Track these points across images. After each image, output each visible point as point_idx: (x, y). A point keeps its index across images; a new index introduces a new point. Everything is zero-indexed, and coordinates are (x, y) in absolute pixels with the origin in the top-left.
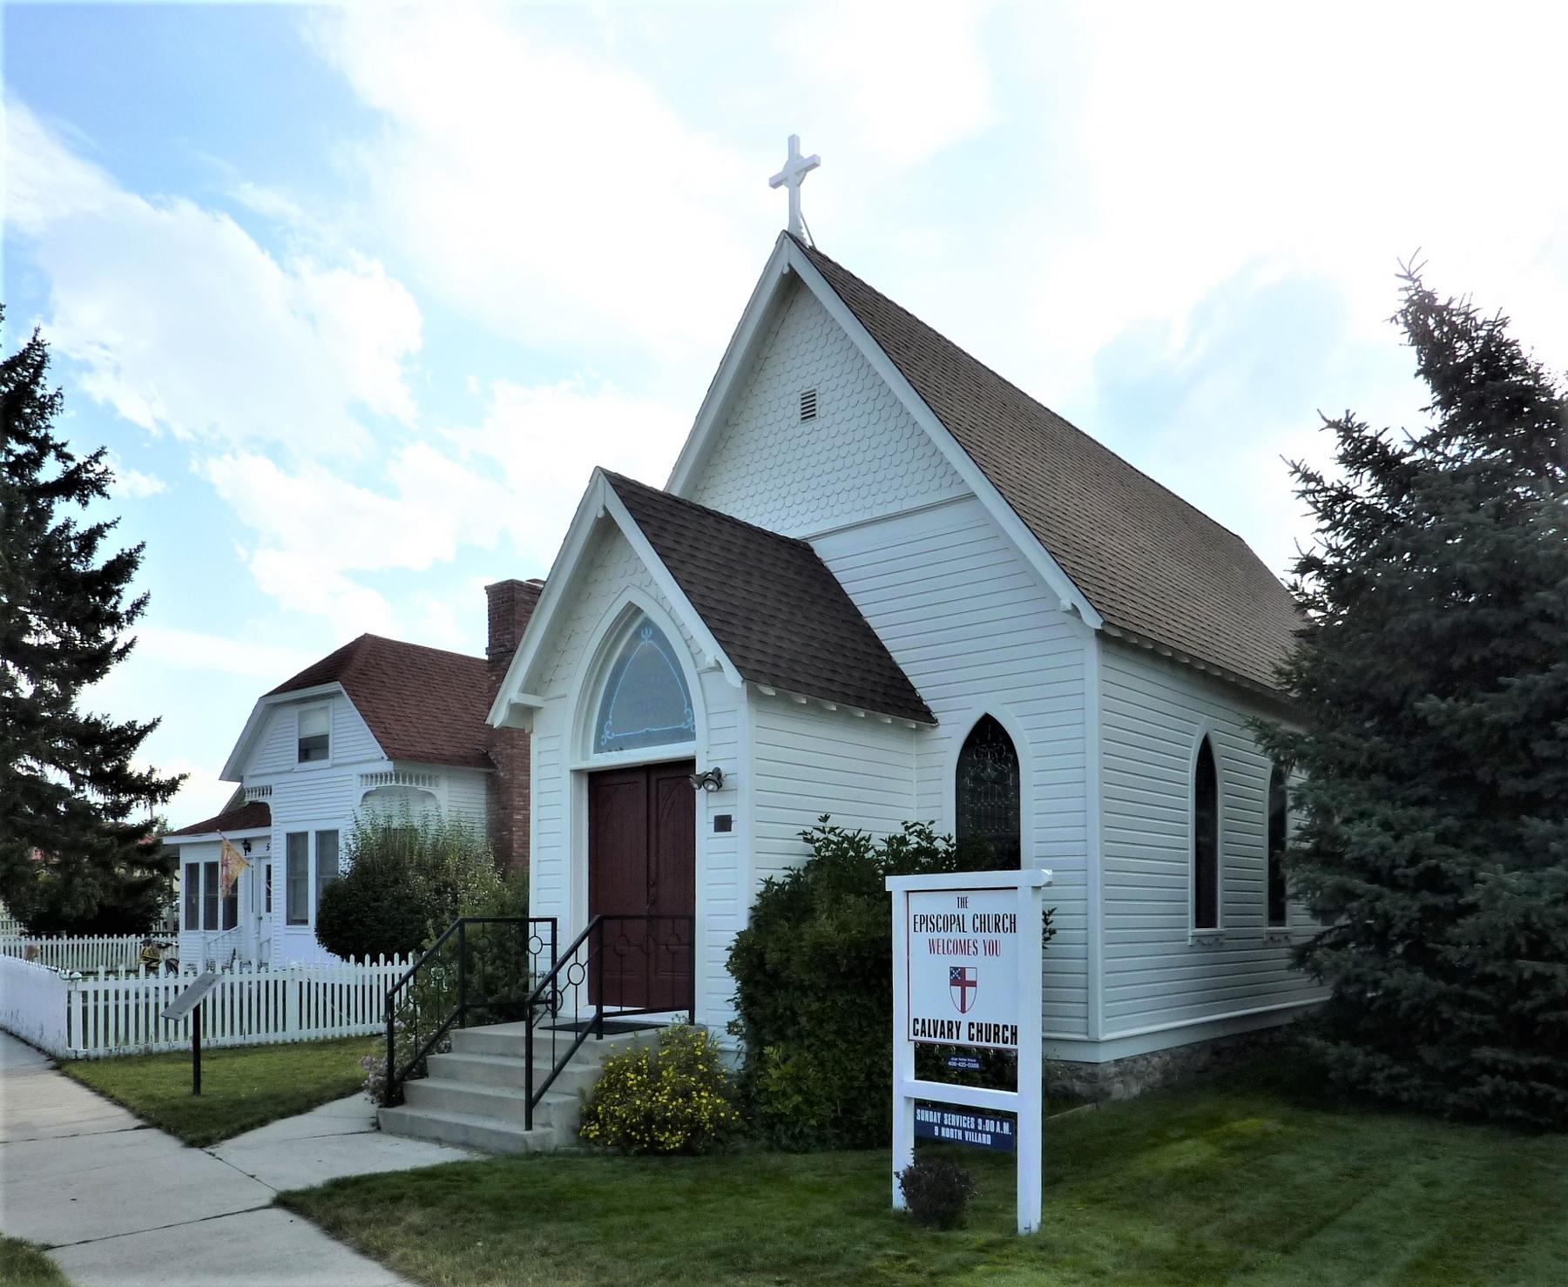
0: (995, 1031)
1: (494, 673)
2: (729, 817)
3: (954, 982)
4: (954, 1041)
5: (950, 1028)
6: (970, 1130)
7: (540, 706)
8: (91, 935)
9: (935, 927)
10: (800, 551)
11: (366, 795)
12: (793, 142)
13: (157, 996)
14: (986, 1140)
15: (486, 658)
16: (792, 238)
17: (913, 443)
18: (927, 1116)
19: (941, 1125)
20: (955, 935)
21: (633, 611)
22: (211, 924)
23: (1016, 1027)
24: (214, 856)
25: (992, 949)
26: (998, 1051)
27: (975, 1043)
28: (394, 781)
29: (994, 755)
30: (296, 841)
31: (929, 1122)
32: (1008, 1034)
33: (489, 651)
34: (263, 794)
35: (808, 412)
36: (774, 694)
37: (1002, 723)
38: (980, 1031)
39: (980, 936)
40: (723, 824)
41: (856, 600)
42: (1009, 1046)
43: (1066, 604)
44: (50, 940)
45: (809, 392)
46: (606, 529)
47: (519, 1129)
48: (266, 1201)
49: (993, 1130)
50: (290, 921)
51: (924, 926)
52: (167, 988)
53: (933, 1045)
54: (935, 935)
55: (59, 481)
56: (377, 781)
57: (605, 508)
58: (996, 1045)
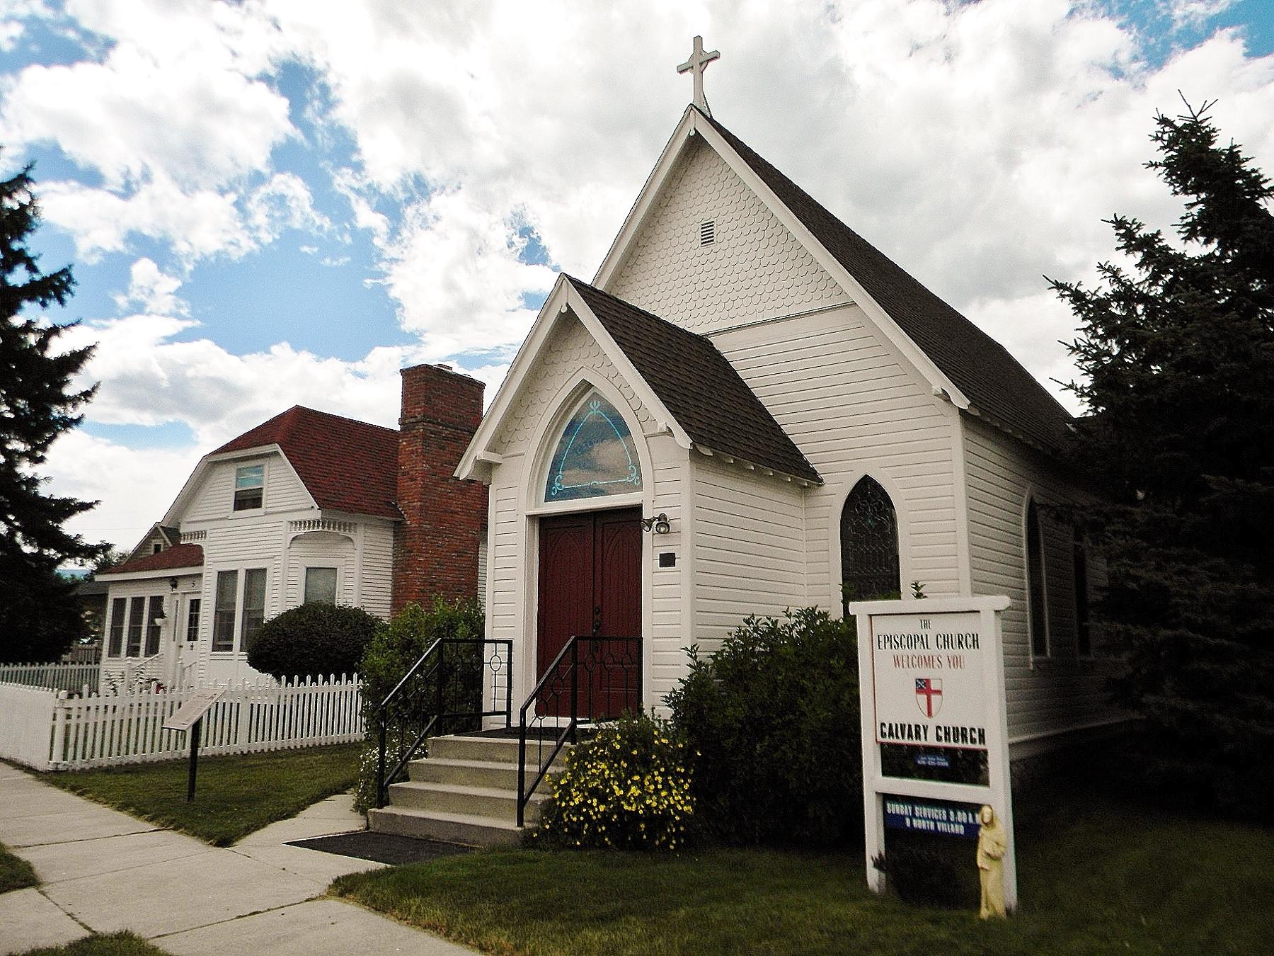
0: (962, 733)
1: (405, 439)
2: (673, 555)
3: (919, 690)
4: (922, 742)
5: (918, 731)
6: (943, 821)
7: (499, 462)
8: (15, 663)
9: (900, 645)
10: (702, 343)
11: (294, 539)
12: (698, 40)
13: (156, 710)
14: (960, 829)
15: (398, 428)
16: (699, 109)
17: (798, 263)
18: (894, 808)
19: (913, 816)
20: (919, 650)
21: (586, 386)
22: (133, 651)
23: (983, 730)
24: (147, 593)
25: (956, 662)
26: (965, 751)
27: (943, 743)
28: (326, 528)
29: (874, 509)
30: (226, 578)
31: (896, 814)
32: (976, 736)
33: (402, 421)
34: (198, 537)
35: (707, 238)
36: (712, 455)
37: (857, 481)
38: (947, 734)
39: (944, 652)
40: (668, 560)
41: (749, 383)
42: (977, 746)
43: (937, 388)
44: (7, 666)
45: (708, 223)
46: (568, 321)
47: (512, 825)
48: (318, 889)
49: (965, 821)
50: (216, 648)
51: (888, 644)
52: (106, 707)
53: (900, 746)
54: (900, 651)
55: (25, 286)
56: (300, 527)
57: (567, 304)
58: (965, 745)
